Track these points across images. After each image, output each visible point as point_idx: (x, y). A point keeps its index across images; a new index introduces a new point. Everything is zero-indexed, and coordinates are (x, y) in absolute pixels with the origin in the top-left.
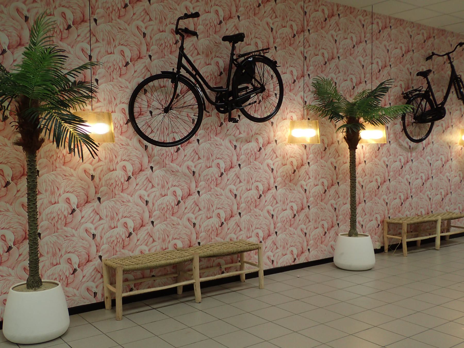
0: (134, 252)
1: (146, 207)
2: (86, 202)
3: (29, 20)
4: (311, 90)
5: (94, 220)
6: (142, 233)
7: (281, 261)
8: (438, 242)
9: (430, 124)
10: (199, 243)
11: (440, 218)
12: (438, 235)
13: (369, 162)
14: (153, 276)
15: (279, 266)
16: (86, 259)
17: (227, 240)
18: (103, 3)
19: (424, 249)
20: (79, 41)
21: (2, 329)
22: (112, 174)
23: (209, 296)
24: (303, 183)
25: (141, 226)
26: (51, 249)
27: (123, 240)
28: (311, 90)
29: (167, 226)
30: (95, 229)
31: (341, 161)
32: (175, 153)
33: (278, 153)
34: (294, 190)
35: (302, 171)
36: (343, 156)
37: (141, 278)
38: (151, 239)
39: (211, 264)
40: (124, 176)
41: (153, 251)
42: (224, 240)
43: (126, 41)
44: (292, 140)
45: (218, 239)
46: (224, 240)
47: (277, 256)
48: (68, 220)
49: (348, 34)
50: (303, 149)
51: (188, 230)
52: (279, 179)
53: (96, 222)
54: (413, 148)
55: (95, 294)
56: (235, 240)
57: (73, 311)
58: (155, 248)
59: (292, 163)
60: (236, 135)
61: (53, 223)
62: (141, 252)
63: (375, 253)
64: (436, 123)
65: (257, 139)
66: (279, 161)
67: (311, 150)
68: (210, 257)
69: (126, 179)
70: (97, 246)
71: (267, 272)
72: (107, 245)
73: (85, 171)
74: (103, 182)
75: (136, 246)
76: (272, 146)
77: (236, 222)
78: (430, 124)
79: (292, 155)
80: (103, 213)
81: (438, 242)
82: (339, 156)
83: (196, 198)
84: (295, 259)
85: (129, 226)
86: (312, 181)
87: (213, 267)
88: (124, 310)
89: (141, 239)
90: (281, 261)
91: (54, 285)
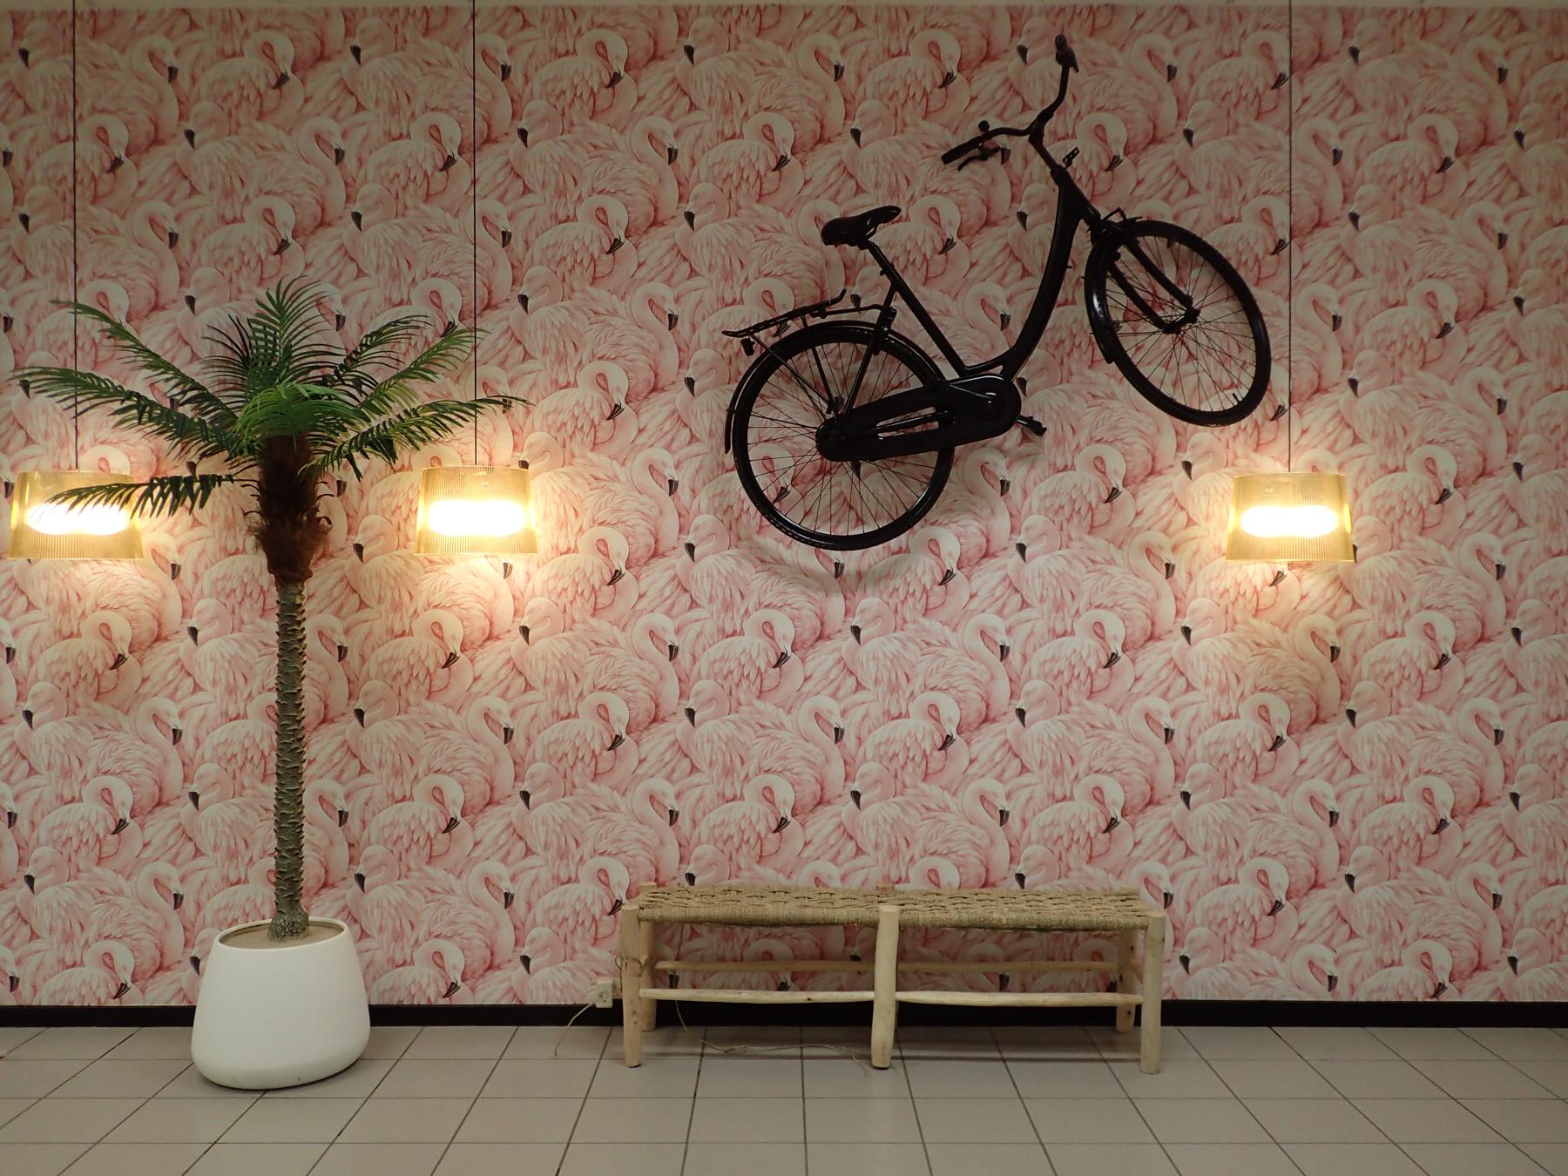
0: (1124, 877)
1: (1166, 747)
2: (324, 721)
3: (1508, 243)
4: (204, 354)
5: (1004, 770)
6: (1152, 825)
7: (55, 983)
8: (883, 1027)
9: (931, 458)
10: (691, 878)
11: (889, 916)
12: (884, 996)
13: (551, 633)
14: (855, 958)
15: (44, 999)
16: (1309, 879)
17: (803, 878)
18: (381, 165)
19: (843, 1050)
20: (1307, 280)
21: (191, 1024)
22: (399, 645)
23: (1105, 1061)
24: (163, 704)
25: (488, 804)
26: (885, 839)
27: (1089, 837)
28: (204, 354)
29: (1234, 811)
30: (1008, 796)
31: (379, 628)
32: (937, 589)
33: (38, 592)
34: (119, 728)
35: (161, 661)
36: (384, 607)
37: (813, 958)
38: (190, 847)
39: (738, 950)
40: (766, 652)
41: (855, 881)
42: (789, 877)
43: (1445, 263)
44: (1241, 549)
45: (767, 873)
46: (789, 877)
47: (1351, 966)
48: (934, 766)
49: (1410, 118)
50: (166, 578)
51: (981, 832)
52: (42, 687)
53: (682, 778)
54: (860, 575)
55: (1332, 980)
56: (836, 884)
57: (382, 1015)
58: (861, 875)
59: (105, 631)
60: (1172, 528)
61: (892, 768)
62: (817, 881)
63: (373, 1023)
64: (969, 457)
65: (934, 541)
66: (43, 620)
67: (206, 583)
68: (729, 923)
69: (774, 662)
70: (1340, 846)
71: (1179, 1013)
72: (712, 847)
73: (1313, 635)
74: (372, 666)
75: (1130, 860)
76: (10, 569)
77: (1500, 825)
78: (931, 458)
79: (104, 601)
80: (1362, 755)
81: (883, 1027)
82: (362, 605)
83: (1009, 732)
84: (122, 989)
85: (1438, 801)
86: (210, 701)
87: (742, 960)
88: (898, 1041)
89: (1147, 841)
90: (55, 983)
91: (328, 931)
